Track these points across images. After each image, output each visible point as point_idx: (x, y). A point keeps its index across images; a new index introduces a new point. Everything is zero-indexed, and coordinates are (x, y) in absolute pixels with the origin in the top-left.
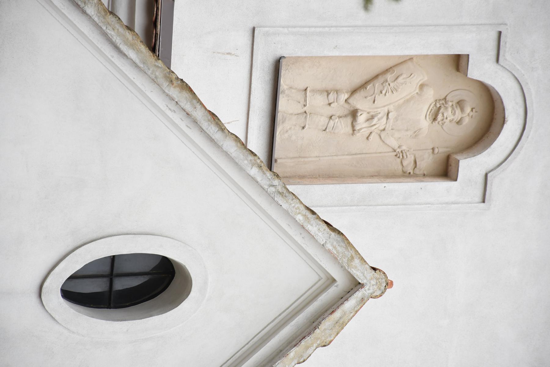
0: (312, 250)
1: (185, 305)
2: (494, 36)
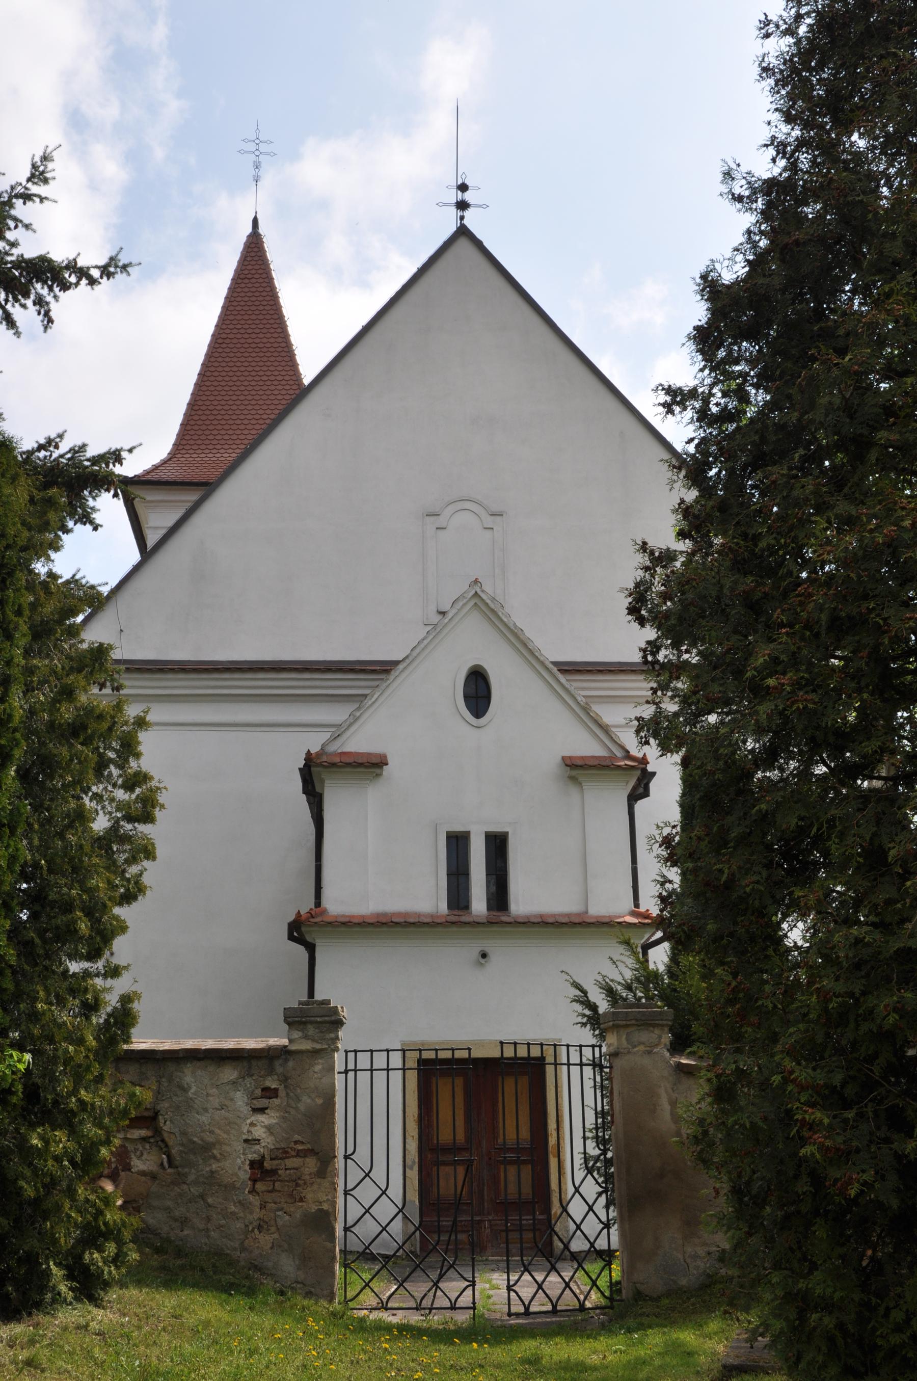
0: (459, 617)
1: (485, 667)
2: (428, 518)
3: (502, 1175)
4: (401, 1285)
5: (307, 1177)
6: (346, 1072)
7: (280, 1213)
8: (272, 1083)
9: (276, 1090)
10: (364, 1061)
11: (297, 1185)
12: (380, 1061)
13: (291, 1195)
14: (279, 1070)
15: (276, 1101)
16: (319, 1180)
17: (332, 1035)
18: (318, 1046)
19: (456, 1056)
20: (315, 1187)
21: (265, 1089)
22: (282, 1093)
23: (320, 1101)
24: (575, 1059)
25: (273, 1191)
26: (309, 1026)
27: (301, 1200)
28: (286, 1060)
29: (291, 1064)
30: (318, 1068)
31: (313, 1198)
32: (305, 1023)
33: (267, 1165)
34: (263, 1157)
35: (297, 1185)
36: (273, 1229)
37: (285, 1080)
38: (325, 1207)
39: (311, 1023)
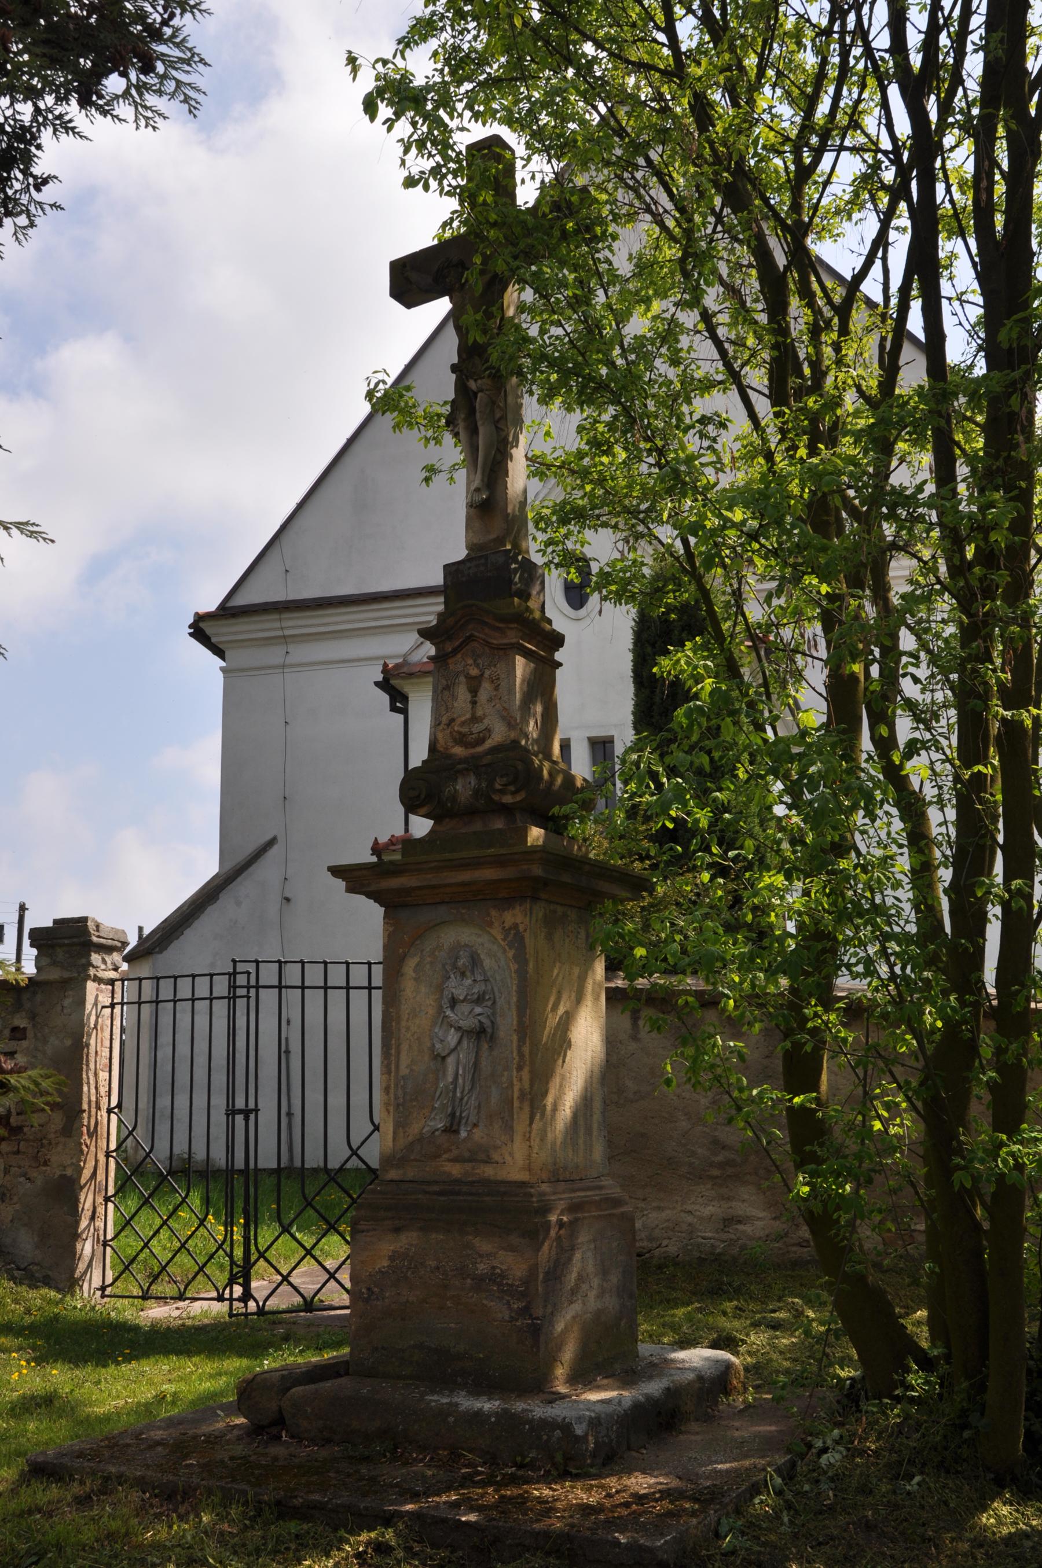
3: (339, 1312)
4: (146, 1202)
5: (52, 1136)
6: (112, 1006)
7: (22, 1179)
8: (20, 1021)
9: (25, 1029)
10: (184, 989)
11: (42, 1146)
12: (202, 988)
13: (36, 1158)
14: (28, 1005)
15: (25, 1044)
16: (62, 1139)
17: (84, 961)
18: (66, 975)
19: (380, 984)
20: (60, 1148)
21: (15, 1029)
22: (30, 1034)
23: (68, 1042)
24: (202, 990)
25: (18, 1152)
26: (58, 950)
27: (45, 1164)
28: (34, 993)
29: (39, 998)
30: (67, 1002)
31: (58, 1157)
32: (52, 946)
33: (14, 1121)
34: (9, 1111)
35: (42, 1146)
36: (15, 1199)
37: (33, 1017)
38: (69, 1172)
39: (61, 946)
